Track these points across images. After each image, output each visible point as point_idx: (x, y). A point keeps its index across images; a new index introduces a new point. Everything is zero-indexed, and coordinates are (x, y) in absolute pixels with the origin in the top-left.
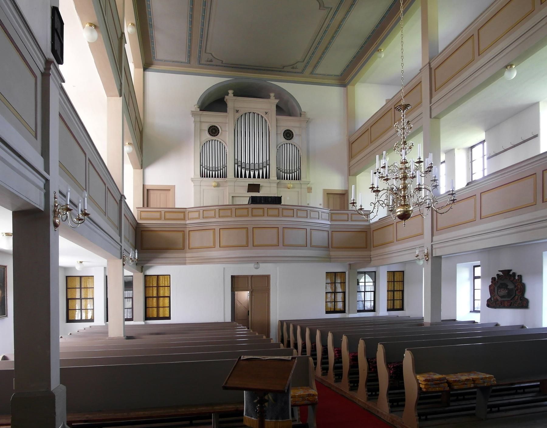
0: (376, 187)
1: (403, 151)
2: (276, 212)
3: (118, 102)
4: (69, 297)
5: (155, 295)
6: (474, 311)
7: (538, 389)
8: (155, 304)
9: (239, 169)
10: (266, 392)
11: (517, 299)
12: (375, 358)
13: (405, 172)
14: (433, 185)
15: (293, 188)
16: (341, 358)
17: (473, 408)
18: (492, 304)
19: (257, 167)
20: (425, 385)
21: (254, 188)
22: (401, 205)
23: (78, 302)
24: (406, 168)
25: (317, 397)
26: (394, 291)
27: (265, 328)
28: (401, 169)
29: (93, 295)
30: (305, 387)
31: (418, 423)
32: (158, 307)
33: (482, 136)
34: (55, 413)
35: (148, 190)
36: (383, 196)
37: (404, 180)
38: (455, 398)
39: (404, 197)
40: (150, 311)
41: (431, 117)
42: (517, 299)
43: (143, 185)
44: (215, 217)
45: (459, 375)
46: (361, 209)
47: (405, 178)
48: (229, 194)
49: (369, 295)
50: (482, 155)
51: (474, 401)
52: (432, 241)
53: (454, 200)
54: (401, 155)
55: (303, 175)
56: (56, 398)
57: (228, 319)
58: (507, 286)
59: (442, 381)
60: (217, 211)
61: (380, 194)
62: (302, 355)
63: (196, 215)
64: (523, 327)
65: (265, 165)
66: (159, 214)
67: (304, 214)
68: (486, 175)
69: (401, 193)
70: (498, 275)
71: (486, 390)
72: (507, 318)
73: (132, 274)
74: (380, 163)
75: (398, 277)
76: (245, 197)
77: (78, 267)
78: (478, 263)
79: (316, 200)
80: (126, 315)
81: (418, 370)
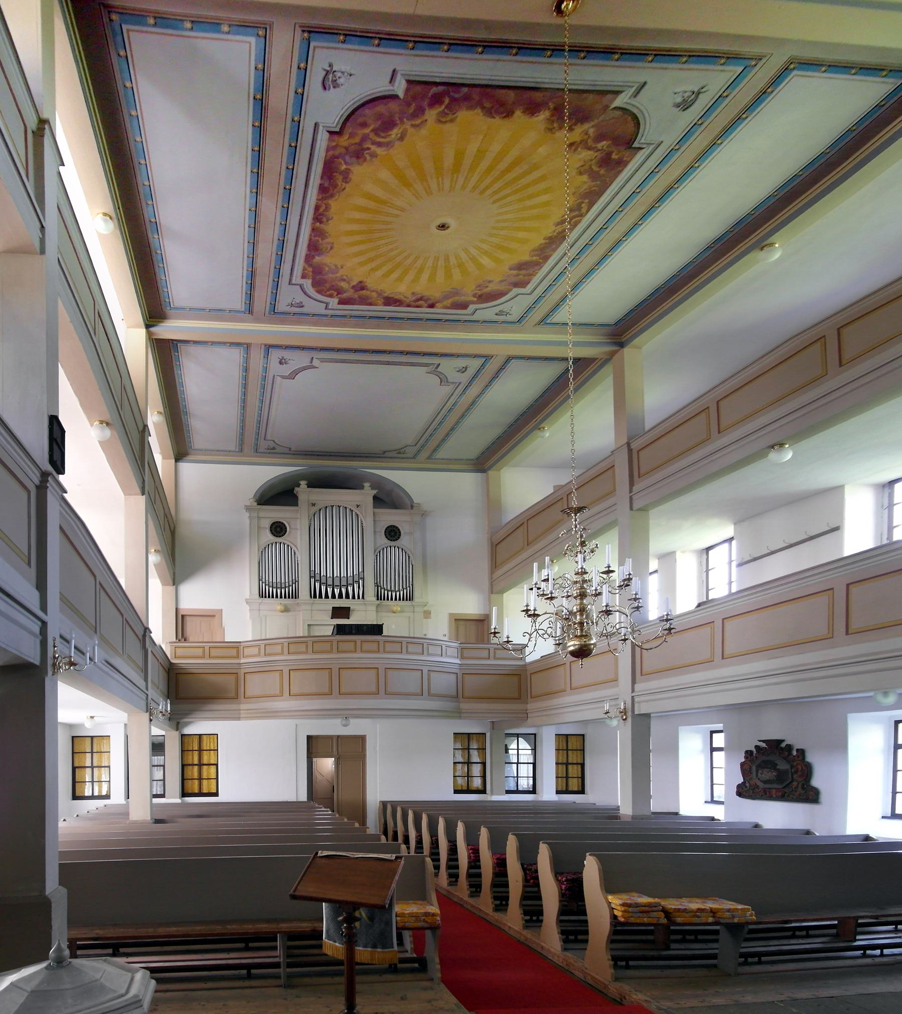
0: (532, 609)
1: (579, 555)
2: (374, 646)
3: (140, 501)
4: (76, 765)
5: (197, 764)
6: (713, 801)
7: (834, 931)
8: (196, 775)
9: (317, 585)
10: (356, 906)
11: (797, 787)
12: (536, 864)
13: (582, 588)
14: (633, 606)
15: (401, 612)
16: (479, 861)
17: (714, 957)
18: (743, 791)
19: (344, 582)
20: (624, 911)
21: (338, 612)
22: (576, 636)
23: (89, 771)
24: (584, 581)
25: (439, 918)
26: (567, 764)
27: (359, 812)
28: (576, 582)
29: (109, 763)
30: (420, 902)
31: (613, 971)
32: (200, 779)
33: (729, 530)
34: (51, 927)
35: (183, 616)
36: (544, 623)
37: (582, 599)
38: (679, 937)
39: (581, 624)
40: (188, 784)
41: (631, 509)
42: (797, 787)
43: (177, 609)
44: (282, 653)
45: (684, 900)
46: (508, 642)
47: (582, 595)
48: (304, 622)
49: (526, 770)
50: (727, 560)
51: (715, 945)
52: (633, 691)
53: (670, 629)
54: (577, 562)
55: (416, 594)
56: (53, 906)
57: (303, 797)
58: (777, 765)
59: (654, 909)
60: (286, 645)
61: (540, 619)
62: (416, 852)
63: (255, 651)
64: (808, 832)
65: (356, 579)
66: (201, 650)
67: (419, 649)
68: (734, 590)
69: (576, 618)
70: (756, 747)
71: (735, 929)
72: (776, 816)
73: (163, 733)
74: (540, 576)
75: (573, 744)
76: (326, 625)
77: (88, 724)
78: (720, 726)
79: (438, 628)
80: (154, 790)
81: (609, 886)
